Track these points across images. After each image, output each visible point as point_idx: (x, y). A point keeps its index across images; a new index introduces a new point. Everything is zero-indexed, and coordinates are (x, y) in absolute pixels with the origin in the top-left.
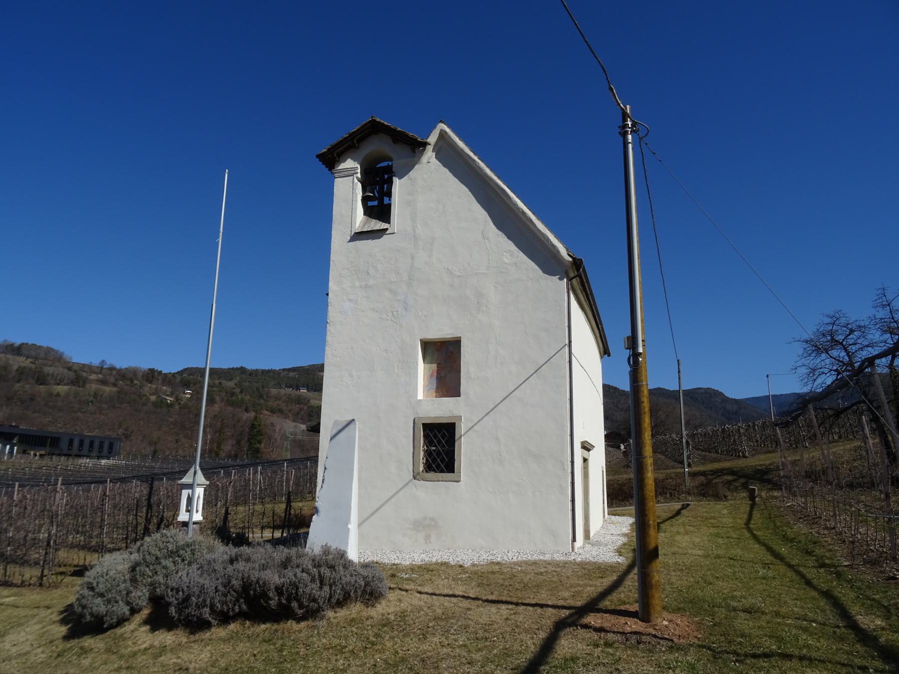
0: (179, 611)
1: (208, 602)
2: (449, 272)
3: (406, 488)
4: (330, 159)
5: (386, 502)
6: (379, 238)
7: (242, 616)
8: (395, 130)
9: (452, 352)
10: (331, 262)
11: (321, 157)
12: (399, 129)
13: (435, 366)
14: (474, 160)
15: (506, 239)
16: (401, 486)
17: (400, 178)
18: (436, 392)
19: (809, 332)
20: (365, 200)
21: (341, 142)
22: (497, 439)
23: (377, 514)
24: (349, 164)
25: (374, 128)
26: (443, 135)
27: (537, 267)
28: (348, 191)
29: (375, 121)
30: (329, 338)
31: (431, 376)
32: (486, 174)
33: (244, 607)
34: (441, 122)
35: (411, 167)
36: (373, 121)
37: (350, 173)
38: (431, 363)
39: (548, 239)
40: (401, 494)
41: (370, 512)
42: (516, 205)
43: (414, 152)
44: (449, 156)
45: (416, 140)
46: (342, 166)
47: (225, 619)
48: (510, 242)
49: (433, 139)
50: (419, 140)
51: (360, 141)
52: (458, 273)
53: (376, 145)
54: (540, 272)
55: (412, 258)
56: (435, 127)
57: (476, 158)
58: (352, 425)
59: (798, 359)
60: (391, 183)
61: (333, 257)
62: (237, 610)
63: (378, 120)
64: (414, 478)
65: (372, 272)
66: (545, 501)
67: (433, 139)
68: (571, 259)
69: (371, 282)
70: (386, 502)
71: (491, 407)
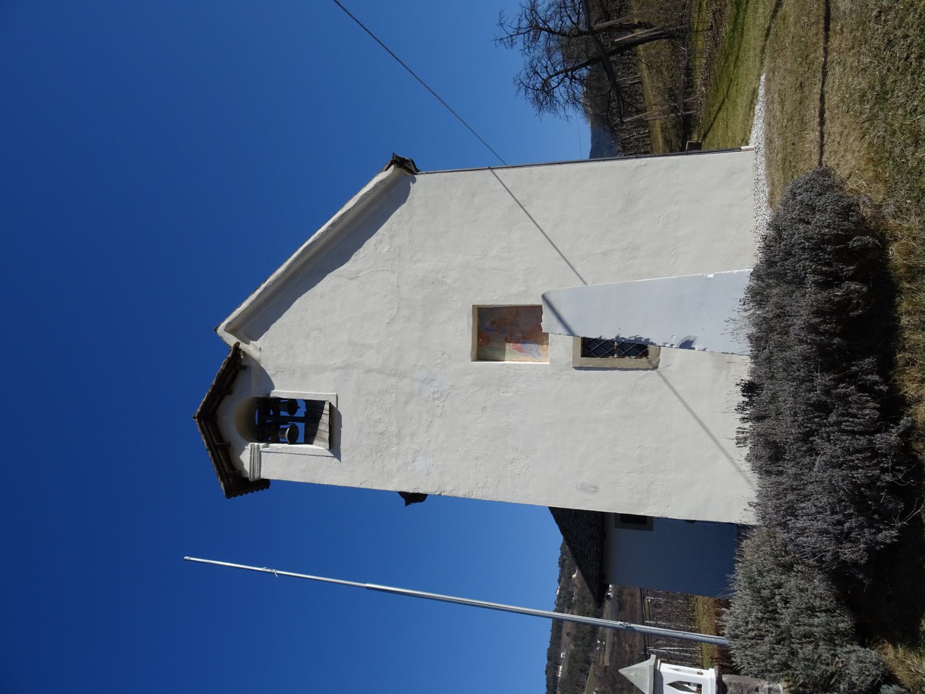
0: (887, 518)
1: (863, 441)
2: (392, 321)
3: (670, 381)
4: (240, 484)
5: (690, 410)
6: (340, 417)
7: (887, 366)
8: (214, 388)
9: (493, 323)
10: (363, 486)
11: (231, 492)
12: (214, 383)
13: (509, 347)
14: (266, 288)
15: (361, 249)
16: (666, 387)
17: (273, 388)
18: (542, 344)
19: (530, 109)
20: (293, 440)
21: (216, 462)
22: (605, 254)
23: (707, 424)
24: (245, 457)
25: (209, 418)
26: (232, 330)
27: (398, 211)
28: (278, 462)
29: (199, 414)
30: (460, 493)
31: (521, 350)
32: (284, 273)
33: (868, 362)
34: (216, 330)
35: (262, 371)
36: (200, 417)
37: (256, 455)
38: (504, 350)
39: (367, 194)
40: (678, 388)
41: (703, 433)
42: (322, 235)
43: (245, 368)
44: (257, 323)
45: (230, 360)
46: (247, 467)
47: (893, 406)
48: (365, 245)
49: (231, 340)
50: (230, 355)
51: (220, 438)
52: (395, 311)
53: (232, 416)
54: (404, 206)
55: (369, 371)
56: (221, 338)
57: (263, 286)
58: (551, 298)
59: (558, 116)
60: (278, 400)
61: (356, 484)
62: (876, 378)
63: (199, 410)
64: (656, 368)
65: (381, 428)
66: (690, 233)
67: (231, 340)
68: (393, 167)
69: (393, 429)
70: (690, 410)
71: (564, 263)
